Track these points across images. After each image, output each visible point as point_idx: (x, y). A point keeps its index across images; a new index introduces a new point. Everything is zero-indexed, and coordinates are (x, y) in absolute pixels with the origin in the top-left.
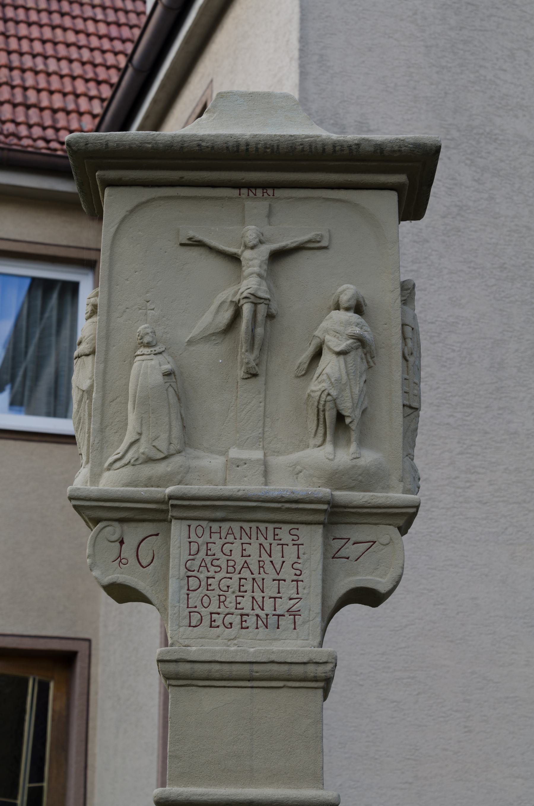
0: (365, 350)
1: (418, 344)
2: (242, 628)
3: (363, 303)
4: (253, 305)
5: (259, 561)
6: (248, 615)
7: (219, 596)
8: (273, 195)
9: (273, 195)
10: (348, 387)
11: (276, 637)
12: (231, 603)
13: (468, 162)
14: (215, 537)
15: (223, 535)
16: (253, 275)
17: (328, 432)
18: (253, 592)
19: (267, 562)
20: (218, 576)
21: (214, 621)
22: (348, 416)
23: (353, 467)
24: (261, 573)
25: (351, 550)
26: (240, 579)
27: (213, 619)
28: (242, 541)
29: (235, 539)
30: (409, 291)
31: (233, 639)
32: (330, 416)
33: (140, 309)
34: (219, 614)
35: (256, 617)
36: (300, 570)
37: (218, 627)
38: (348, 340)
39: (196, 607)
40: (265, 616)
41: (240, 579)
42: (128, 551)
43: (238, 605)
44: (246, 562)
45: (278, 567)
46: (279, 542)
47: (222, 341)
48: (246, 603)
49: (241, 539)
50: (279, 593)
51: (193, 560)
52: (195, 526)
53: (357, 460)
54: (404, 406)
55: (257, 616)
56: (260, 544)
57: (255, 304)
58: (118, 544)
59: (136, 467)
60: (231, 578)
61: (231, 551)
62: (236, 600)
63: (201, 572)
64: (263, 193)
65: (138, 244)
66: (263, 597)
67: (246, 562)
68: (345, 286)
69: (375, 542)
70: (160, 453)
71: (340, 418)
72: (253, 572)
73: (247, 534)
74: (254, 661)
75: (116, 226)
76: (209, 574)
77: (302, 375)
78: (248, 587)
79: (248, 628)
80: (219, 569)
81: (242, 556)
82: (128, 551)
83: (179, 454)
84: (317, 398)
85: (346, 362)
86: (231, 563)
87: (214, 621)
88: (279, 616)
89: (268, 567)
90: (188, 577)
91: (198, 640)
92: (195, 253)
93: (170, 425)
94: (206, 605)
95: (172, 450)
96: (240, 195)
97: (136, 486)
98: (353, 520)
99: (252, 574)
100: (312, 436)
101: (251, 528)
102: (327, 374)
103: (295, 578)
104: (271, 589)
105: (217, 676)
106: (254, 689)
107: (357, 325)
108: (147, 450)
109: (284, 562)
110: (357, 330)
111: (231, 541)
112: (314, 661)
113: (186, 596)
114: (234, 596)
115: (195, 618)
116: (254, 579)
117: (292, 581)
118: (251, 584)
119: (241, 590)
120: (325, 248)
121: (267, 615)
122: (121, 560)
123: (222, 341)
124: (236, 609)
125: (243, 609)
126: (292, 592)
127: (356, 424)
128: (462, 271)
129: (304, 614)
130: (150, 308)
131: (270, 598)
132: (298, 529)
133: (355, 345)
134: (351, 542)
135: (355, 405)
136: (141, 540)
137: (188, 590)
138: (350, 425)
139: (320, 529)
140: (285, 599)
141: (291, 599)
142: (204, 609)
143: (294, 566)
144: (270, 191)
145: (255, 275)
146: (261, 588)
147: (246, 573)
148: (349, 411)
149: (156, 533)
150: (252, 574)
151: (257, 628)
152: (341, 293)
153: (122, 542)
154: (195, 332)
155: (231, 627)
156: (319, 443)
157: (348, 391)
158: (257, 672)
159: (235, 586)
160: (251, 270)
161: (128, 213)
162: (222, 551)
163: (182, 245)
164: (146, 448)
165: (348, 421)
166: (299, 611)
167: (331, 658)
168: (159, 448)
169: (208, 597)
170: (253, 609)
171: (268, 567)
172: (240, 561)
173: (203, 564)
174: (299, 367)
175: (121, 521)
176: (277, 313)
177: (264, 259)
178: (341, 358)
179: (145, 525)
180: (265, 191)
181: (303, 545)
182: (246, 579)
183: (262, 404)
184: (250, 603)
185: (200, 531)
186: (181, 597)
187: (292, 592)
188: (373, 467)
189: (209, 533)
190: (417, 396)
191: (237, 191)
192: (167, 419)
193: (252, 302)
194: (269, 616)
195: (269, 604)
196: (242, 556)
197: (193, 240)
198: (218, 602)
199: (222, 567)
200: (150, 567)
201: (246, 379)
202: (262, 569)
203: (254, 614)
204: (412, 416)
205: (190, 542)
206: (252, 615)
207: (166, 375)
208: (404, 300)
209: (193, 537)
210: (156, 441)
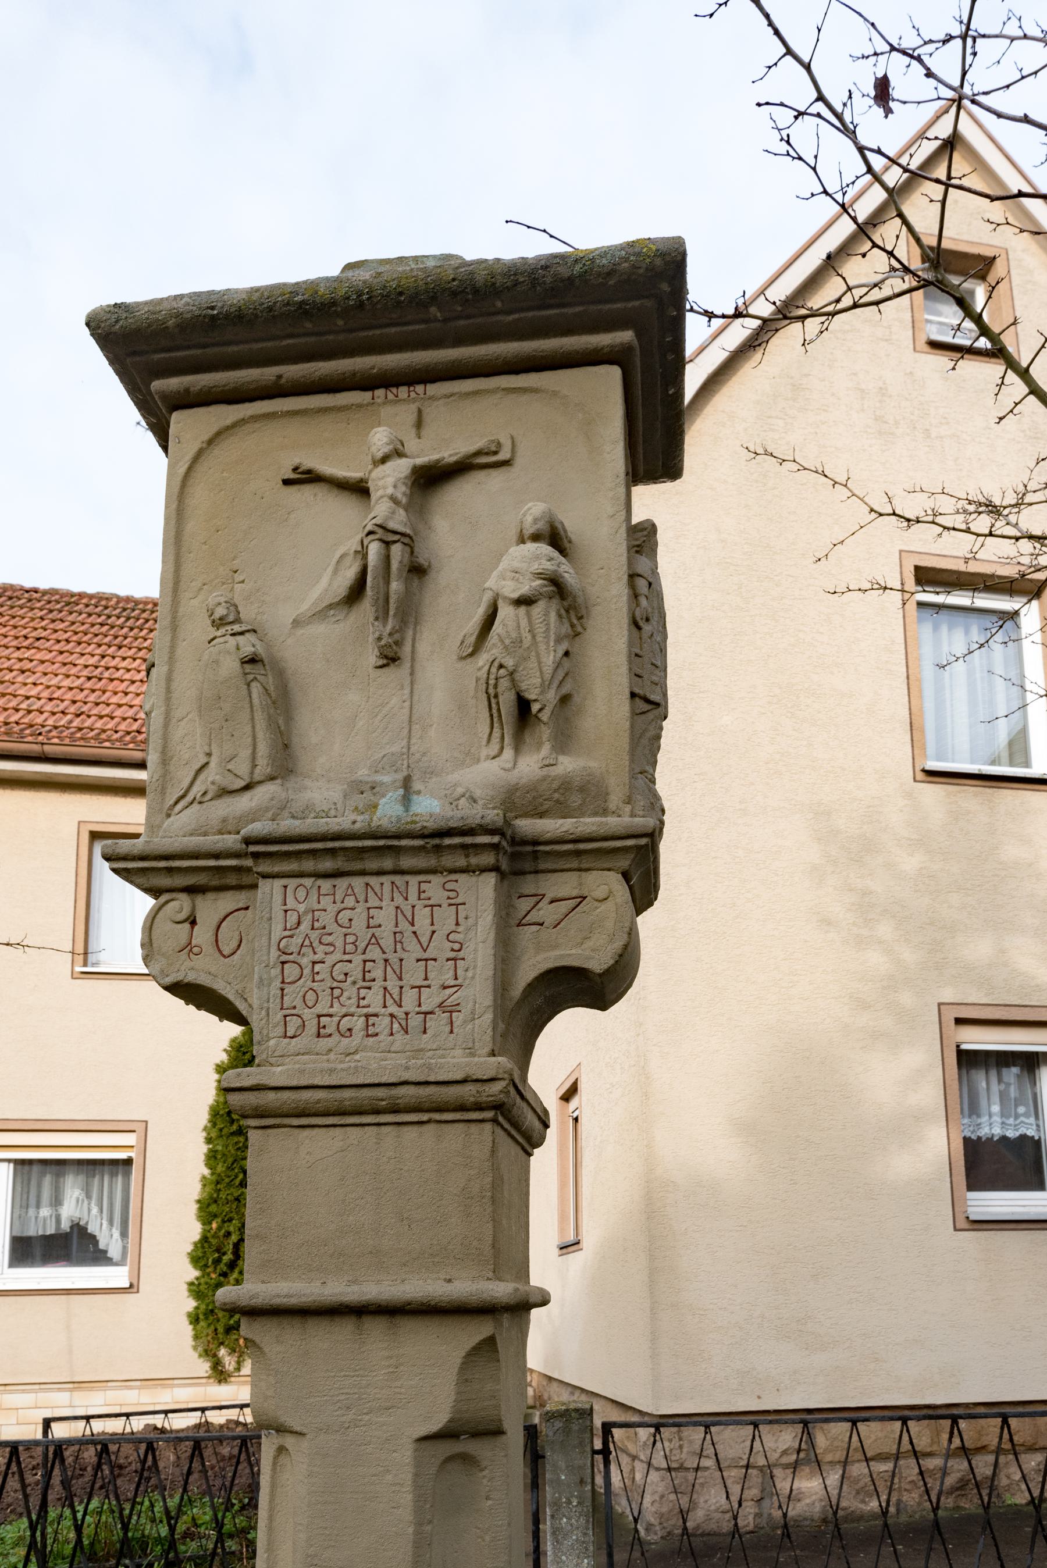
0: (565, 603)
1: (659, 612)
2: (368, 1036)
3: (562, 533)
4: (383, 545)
5: (395, 933)
6: (376, 1015)
7: (332, 989)
8: (425, 394)
9: (425, 394)
10: (533, 653)
11: (422, 1046)
12: (350, 998)
13: (789, 715)
14: (326, 901)
15: (338, 898)
16: (382, 500)
17: (506, 735)
18: (385, 980)
19: (408, 934)
20: (330, 960)
21: (324, 1027)
22: (535, 700)
23: (544, 779)
24: (398, 950)
25: (546, 912)
26: (365, 961)
27: (321, 1025)
28: (369, 905)
29: (358, 902)
30: (645, 533)
31: (353, 1053)
32: (507, 701)
33: (223, 583)
34: (331, 1016)
35: (390, 1018)
36: (460, 943)
37: (330, 1035)
38: (534, 581)
39: (295, 1008)
40: (404, 1016)
41: (365, 961)
42: (202, 935)
43: (361, 1001)
44: (373, 935)
45: (424, 940)
46: (427, 902)
47: (346, 617)
48: (374, 999)
49: (366, 901)
50: (426, 979)
51: (291, 936)
52: (296, 886)
53: (551, 768)
54: (633, 695)
55: (392, 1015)
56: (397, 908)
57: (387, 544)
58: (187, 925)
59: (205, 805)
60: (350, 961)
61: (350, 920)
62: (359, 993)
63: (304, 955)
64: (409, 392)
65: (222, 490)
66: (401, 987)
67: (373, 935)
68: (530, 505)
69: (585, 898)
70: (239, 780)
71: (523, 706)
72: (385, 950)
73: (376, 894)
74: (377, 1082)
75: (186, 466)
76: (316, 958)
77: (468, 655)
78: (377, 973)
79: (377, 1035)
80: (332, 949)
81: (368, 927)
82: (202, 935)
83: (271, 782)
84: (485, 676)
85: (529, 615)
86: (350, 939)
87: (324, 1027)
88: (426, 1013)
89: (411, 944)
90: (283, 963)
91: (298, 1057)
92: (307, 492)
93: (254, 738)
94: (310, 1004)
95: (259, 774)
96: (373, 399)
97: (205, 834)
98: (549, 865)
99: (384, 953)
100: (484, 742)
101: (382, 884)
102: (499, 635)
103: (452, 955)
104: (414, 975)
105: (321, 1109)
106: (383, 1128)
107: (551, 559)
108: (218, 777)
109: (434, 932)
110: (549, 566)
111: (351, 905)
112: (475, 1077)
113: (280, 992)
114: (354, 989)
115: (293, 1024)
116: (386, 961)
117: (448, 960)
118: (383, 968)
119: (367, 978)
120: (506, 463)
121: (407, 1014)
122: (191, 948)
123: (346, 617)
124: (358, 1007)
125: (369, 1006)
126: (447, 976)
127: (549, 713)
128: (784, 807)
129: (466, 1008)
130: (237, 580)
131: (412, 988)
132: (456, 881)
133: (545, 589)
134: (546, 900)
135: (547, 683)
136: (222, 918)
137: (283, 982)
138: (540, 715)
139: (490, 880)
140: (434, 988)
141: (445, 988)
142: (307, 1010)
143: (451, 937)
144: (420, 388)
145: (385, 499)
146: (398, 972)
147: (374, 953)
148: (537, 691)
149: (244, 906)
150: (384, 953)
151: (392, 1034)
152: (524, 515)
153: (193, 923)
154: (305, 606)
155: (351, 1035)
156: (493, 753)
157: (533, 659)
158: (382, 1100)
159: (356, 973)
160: (380, 493)
161: (204, 445)
162: (336, 921)
163: (287, 482)
164: (217, 774)
165: (535, 707)
166: (458, 1004)
167: (501, 1071)
168: (236, 772)
169: (314, 991)
170: (385, 1007)
171: (411, 944)
172: (365, 936)
173: (307, 943)
174: (462, 642)
175: (191, 890)
176: (430, 563)
177: (402, 475)
178: (522, 610)
179: (229, 894)
180: (412, 388)
181: (464, 904)
182: (374, 961)
183: (407, 704)
184: (380, 997)
185: (301, 894)
186: (272, 993)
187: (447, 976)
188: (578, 779)
189: (317, 896)
190: (657, 684)
191: (368, 395)
192: (248, 729)
193: (380, 540)
194: (409, 1016)
195: (409, 998)
196: (368, 927)
197: (300, 470)
198: (330, 998)
199: (337, 945)
200: (235, 956)
201: (381, 667)
202: (399, 946)
203: (387, 1013)
204: (651, 716)
205: (286, 911)
206: (384, 1015)
207: (246, 662)
208: (638, 546)
209: (291, 903)
210: (233, 762)
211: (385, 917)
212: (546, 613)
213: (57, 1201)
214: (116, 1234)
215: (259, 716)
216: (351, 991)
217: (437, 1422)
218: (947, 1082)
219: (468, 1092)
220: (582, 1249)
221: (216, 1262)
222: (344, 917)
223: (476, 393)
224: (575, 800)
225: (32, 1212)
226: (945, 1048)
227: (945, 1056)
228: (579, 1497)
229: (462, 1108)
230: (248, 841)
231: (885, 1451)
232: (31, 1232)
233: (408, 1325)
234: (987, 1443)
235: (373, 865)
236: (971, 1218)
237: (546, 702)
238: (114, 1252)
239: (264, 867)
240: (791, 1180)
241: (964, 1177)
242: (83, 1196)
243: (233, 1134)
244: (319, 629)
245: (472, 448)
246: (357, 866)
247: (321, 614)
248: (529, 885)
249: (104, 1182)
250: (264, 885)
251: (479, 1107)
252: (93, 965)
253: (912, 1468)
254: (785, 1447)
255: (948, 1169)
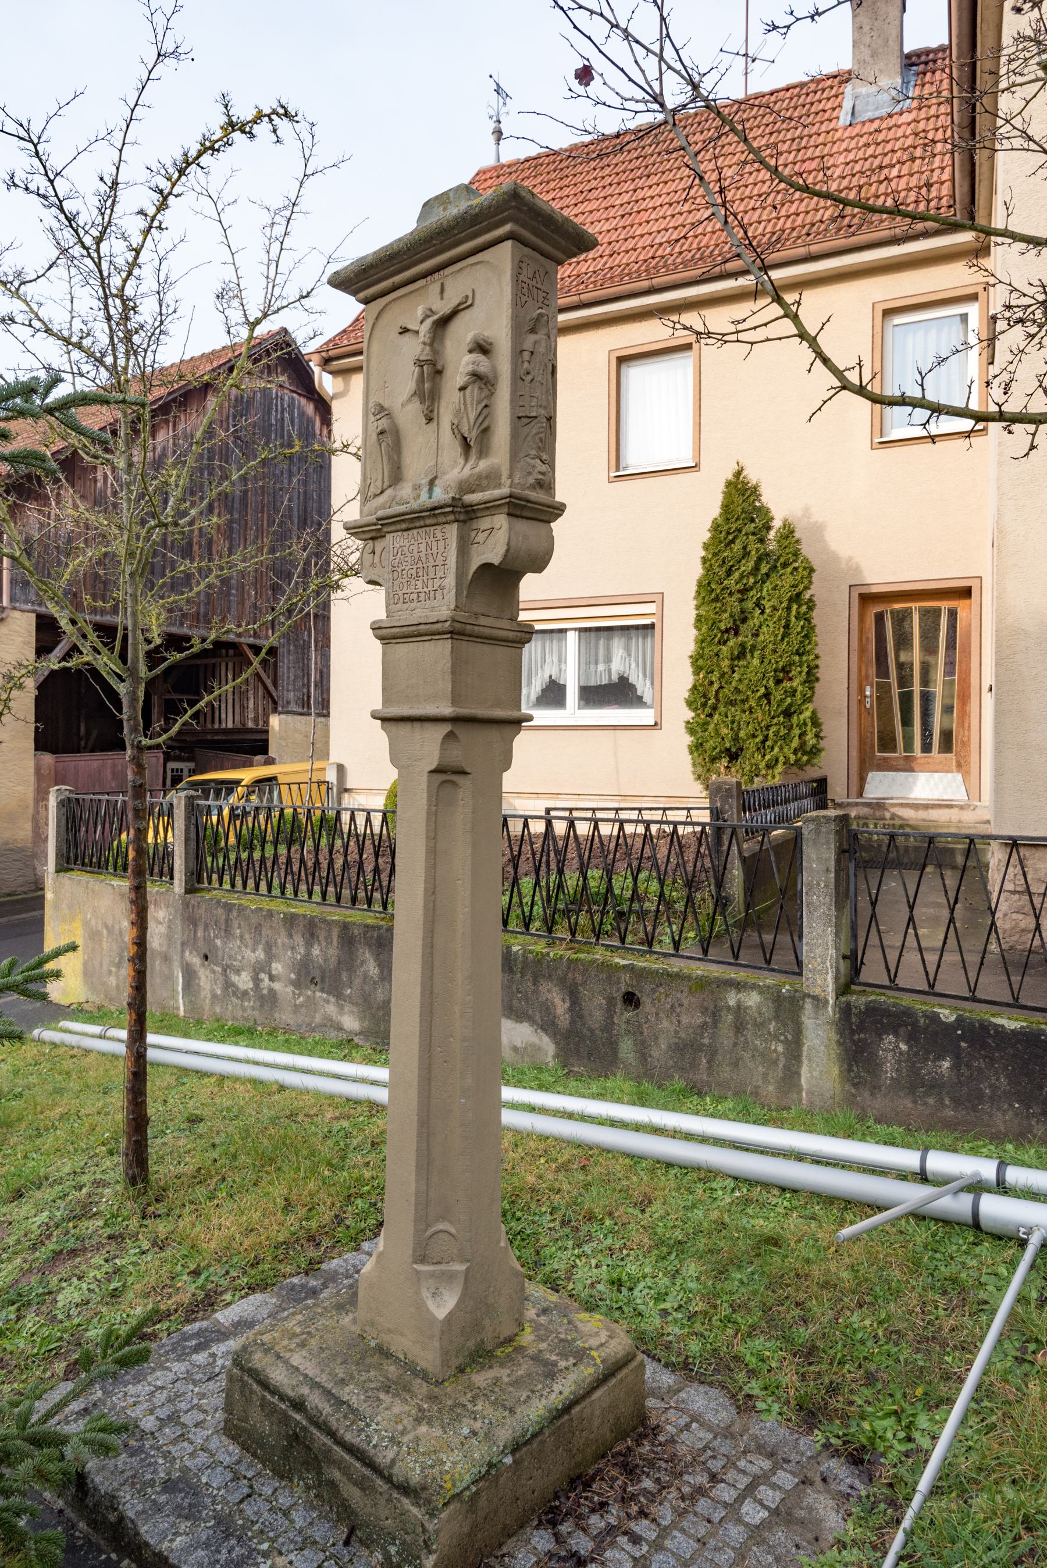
25: (481, 537)
175: (373, 539)
211: (423, 547)
213: (608, 660)
214: (648, 683)
215: (385, 458)
217: (433, 767)
219: (439, 626)
221: (704, 705)
224: (485, 483)
225: (592, 666)
228: (825, 882)
229: (439, 634)
230: (379, 519)
232: (592, 683)
233: (427, 725)
235: (417, 524)
238: (647, 698)
239: (385, 529)
242: (625, 654)
243: (713, 601)
244: (409, 407)
245: (456, 303)
248: (475, 524)
249: (637, 642)
252: (625, 468)
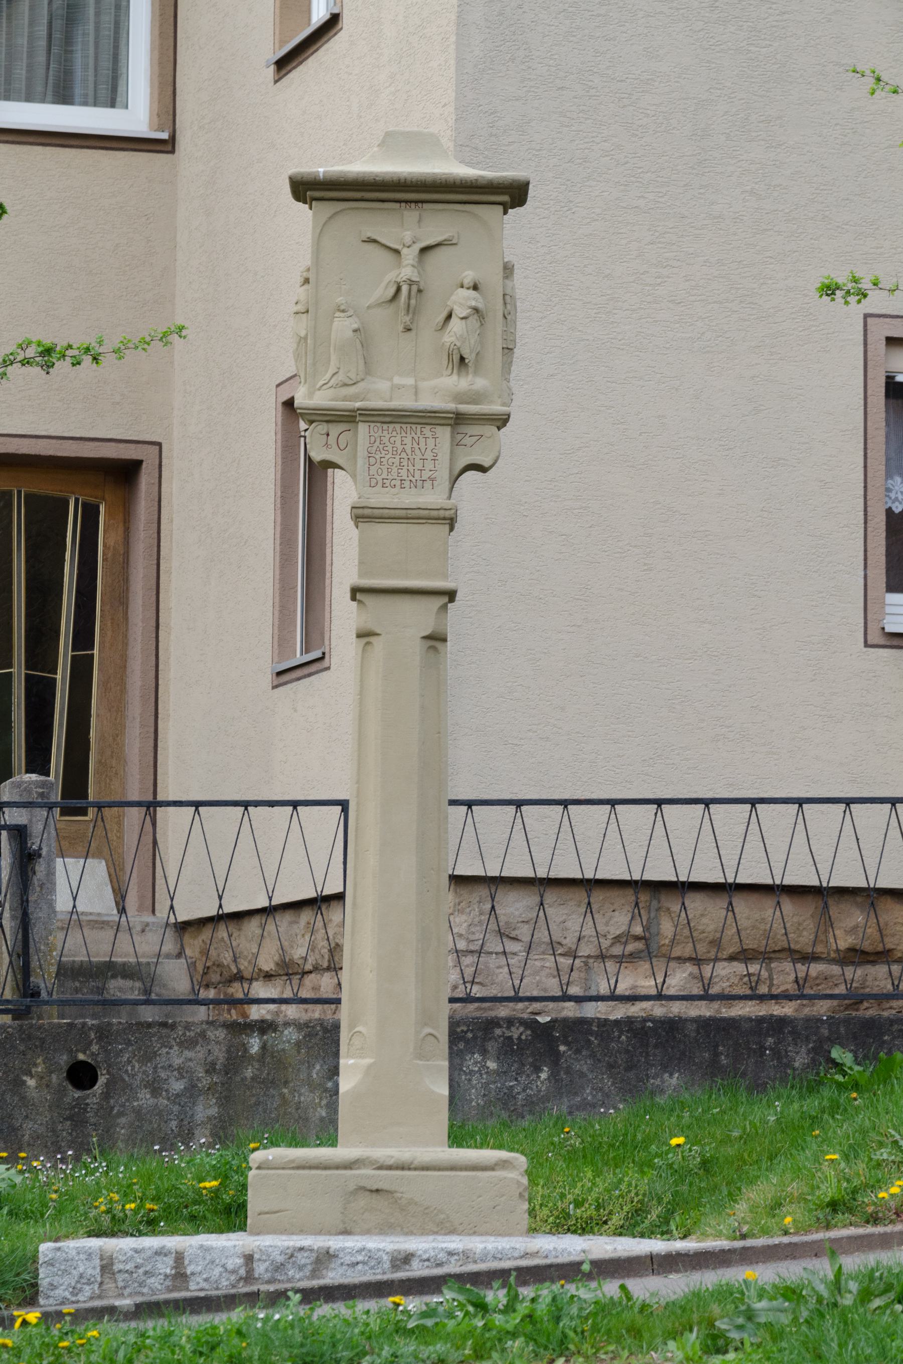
14: (385, 432)
25: (468, 441)
32: (456, 358)
45: (423, 451)
48: (404, 473)
57: (410, 285)
71: (462, 359)
78: (405, 463)
89: (417, 451)
92: (371, 247)
104: (419, 465)
115: (373, 482)
139: (449, 429)
153: (328, 435)
154: (372, 300)
165: (467, 361)
172: (400, 448)
175: (327, 422)
179: (342, 424)
195: (417, 473)
211: (408, 441)
212: (474, 321)
216: (395, 470)
218: (869, 431)
219: (442, 513)
220: (328, 668)
222: (392, 440)
223: (443, 210)
226: (869, 381)
227: (869, 392)
231: (751, 946)
234: (893, 947)
236: (887, 630)
237: (470, 357)
240: (645, 564)
241: (884, 571)
246: (399, 420)
247: (380, 305)
250: (361, 425)
251: (444, 519)
253: (788, 974)
254: (618, 933)
255: (862, 558)
